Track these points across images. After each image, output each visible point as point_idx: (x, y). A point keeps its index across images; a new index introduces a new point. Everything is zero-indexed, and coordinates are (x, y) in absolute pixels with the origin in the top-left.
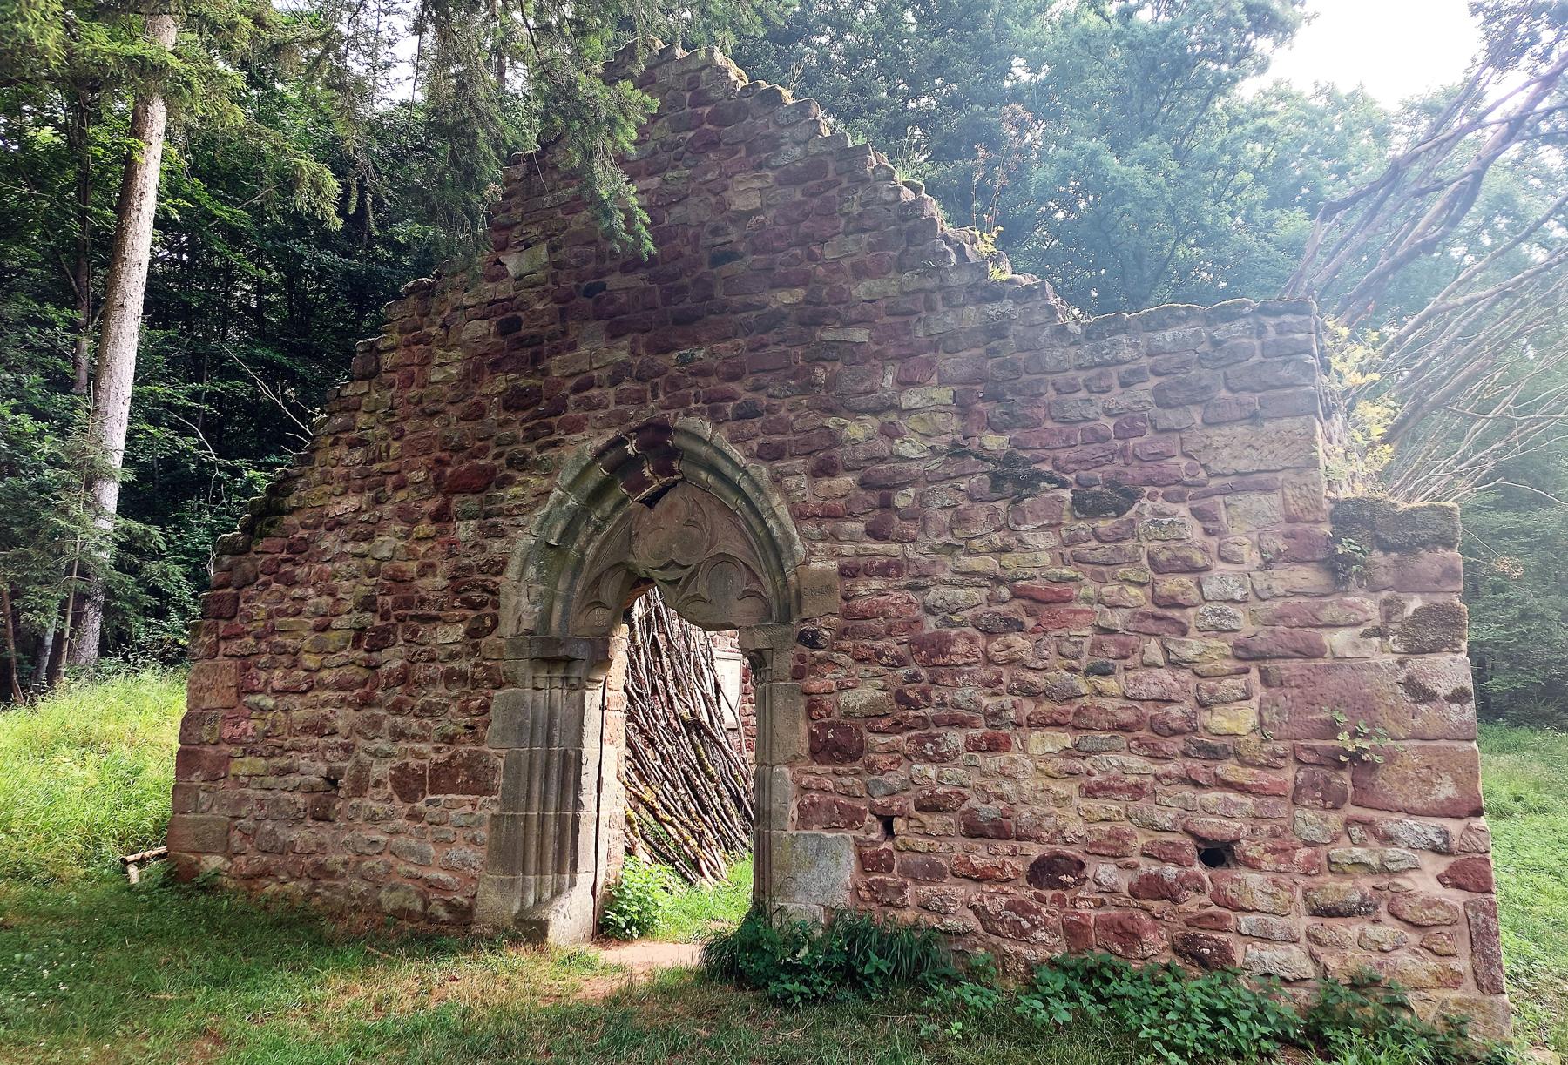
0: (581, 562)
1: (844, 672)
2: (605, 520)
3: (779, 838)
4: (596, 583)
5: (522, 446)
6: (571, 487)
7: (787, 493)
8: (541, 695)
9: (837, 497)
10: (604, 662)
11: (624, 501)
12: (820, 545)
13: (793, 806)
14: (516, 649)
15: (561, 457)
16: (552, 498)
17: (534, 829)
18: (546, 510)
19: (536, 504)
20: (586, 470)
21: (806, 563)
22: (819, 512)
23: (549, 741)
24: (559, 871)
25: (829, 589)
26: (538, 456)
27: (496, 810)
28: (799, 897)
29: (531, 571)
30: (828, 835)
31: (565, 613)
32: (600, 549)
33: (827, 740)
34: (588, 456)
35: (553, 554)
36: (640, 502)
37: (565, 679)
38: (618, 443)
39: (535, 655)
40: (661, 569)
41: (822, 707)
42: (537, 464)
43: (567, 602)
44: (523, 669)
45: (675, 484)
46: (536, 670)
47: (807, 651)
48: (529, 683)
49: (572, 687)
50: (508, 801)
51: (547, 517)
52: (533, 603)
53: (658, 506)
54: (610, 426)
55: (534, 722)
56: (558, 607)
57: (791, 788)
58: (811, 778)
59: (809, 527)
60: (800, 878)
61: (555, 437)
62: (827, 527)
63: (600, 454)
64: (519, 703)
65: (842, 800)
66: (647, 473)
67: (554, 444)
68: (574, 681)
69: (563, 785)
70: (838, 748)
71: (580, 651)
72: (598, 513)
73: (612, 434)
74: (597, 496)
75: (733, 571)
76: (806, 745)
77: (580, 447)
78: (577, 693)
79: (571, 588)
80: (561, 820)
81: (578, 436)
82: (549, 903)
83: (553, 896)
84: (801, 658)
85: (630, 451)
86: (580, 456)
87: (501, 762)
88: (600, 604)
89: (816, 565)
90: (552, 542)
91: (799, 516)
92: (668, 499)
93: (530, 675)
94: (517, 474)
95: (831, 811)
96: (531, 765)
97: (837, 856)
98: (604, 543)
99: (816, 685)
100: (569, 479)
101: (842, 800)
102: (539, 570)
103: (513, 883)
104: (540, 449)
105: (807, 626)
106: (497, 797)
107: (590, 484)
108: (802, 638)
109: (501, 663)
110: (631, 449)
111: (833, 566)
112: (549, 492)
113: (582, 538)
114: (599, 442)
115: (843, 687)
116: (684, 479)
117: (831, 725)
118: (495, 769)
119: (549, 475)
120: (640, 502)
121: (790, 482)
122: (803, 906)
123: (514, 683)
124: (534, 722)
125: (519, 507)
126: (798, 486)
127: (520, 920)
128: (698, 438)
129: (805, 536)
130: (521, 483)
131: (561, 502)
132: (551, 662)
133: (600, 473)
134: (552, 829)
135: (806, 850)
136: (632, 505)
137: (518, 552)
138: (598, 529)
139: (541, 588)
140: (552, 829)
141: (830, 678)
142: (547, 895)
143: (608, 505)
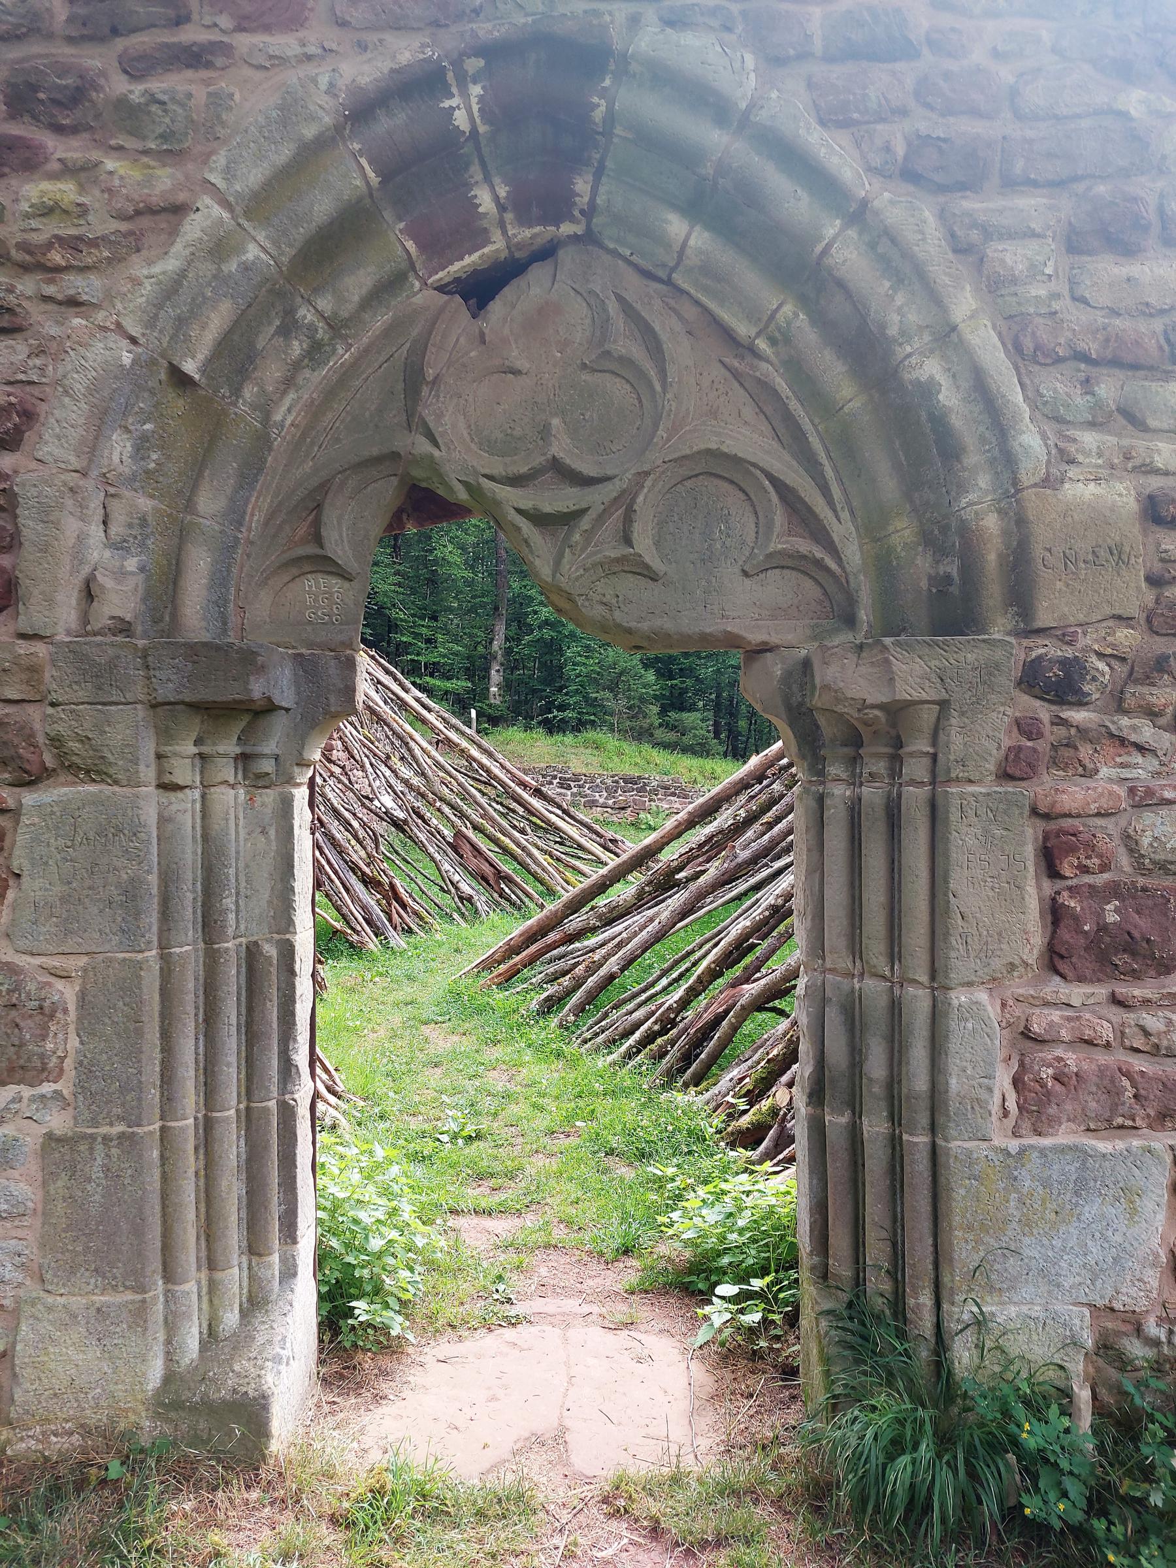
0: (263, 441)
1: (1152, 763)
2: (337, 326)
3: (969, 1159)
4: (313, 506)
5: (65, 52)
6: (258, 206)
7: (995, 286)
8: (186, 805)
9: (1147, 311)
10: (741, 755)
11: (393, 284)
12: (1089, 439)
13: (1003, 1080)
14: (100, 678)
15: (218, 101)
16: (194, 228)
17: (190, 1162)
18: (171, 264)
19: (134, 243)
20: (310, 156)
21: (1049, 482)
22: (1093, 348)
23: (210, 927)
24: (254, 1248)
25: (1118, 554)
26: (136, 92)
27: (58, 1121)
28: (1026, 1292)
29: (119, 450)
30: (1104, 1146)
31: (220, 580)
32: (316, 411)
33: (1103, 928)
34: (323, 111)
35: (178, 404)
36: (441, 289)
37: (245, 759)
38: (423, 84)
39: (166, 692)
40: (515, 481)
41: (1090, 847)
42: (130, 116)
43: (226, 551)
44: (127, 731)
45: (546, 253)
46: (165, 734)
47: (1043, 712)
48: (148, 773)
49: (259, 781)
50: (99, 1090)
51: (171, 289)
52: (119, 546)
53: (496, 307)
54: (398, 26)
55: (168, 879)
56: (199, 565)
57: (998, 1041)
58: (1056, 1015)
59: (1057, 384)
60: (1031, 1249)
61: (191, 35)
62: (1108, 389)
63: (361, 111)
64: (119, 829)
65: (1139, 1064)
66: (485, 201)
67: (195, 58)
68: (268, 766)
69: (251, 1034)
70: (1130, 945)
71: (281, 685)
72: (325, 303)
73: (408, 50)
74: (323, 253)
75: (733, 501)
76: (1038, 940)
77: (292, 77)
78: (269, 797)
79: (235, 515)
80: (250, 1120)
81: (284, 43)
82: (242, 1340)
83: (246, 1314)
84: (1027, 728)
85: (461, 119)
86: (290, 110)
87: (67, 993)
88: (325, 564)
89: (1080, 490)
90: (190, 367)
91: (1028, 355)
92: (533, 288)
93: (148, 748)
94: (51, 142)
95: (1113, 1092)
96: (166, 994)
97: (1129, 1194)
98: (330, 393)
99: (1073, 795)
100: (253, 176)
101: (1139, 1064)
102: (142, 446)
103: (140, 1313)
104: (136, 68)
105: (1050, 649)
106: (64, 1086)
107: (321, 206)
108: (1032, 679)
109: (34, 715)
110: (464, 109)
111: (1122, 496)
112: (178, 210)
113: (271, 372)
114: (362, 71)
115: (1145, 799)
116: (589, 239)
117: (1114, 891)
118: (47, 1013)
119: (172, 155)
120: (441, 289)
121: (1012, 256)
122: (1037, 1311)
123: (95, 772)
124: (168, 879)
125: (74, 244)
126: (1034, 271)
127: (172, 1399)
128: (719, 109)
129: (1054, 416)
130: (68, 170)
131: (219, 247)
132: (215, 713)
133: (353, 174)
134: (232, 1149)
135: (1046, 1184)
136: (421, 296)
137: (79, 383)
138: (316, 352)
139: (145, 504)
140: (232, 1149)
141: (1108, 778)
142: (231, 1319)
143: (357, 283)
